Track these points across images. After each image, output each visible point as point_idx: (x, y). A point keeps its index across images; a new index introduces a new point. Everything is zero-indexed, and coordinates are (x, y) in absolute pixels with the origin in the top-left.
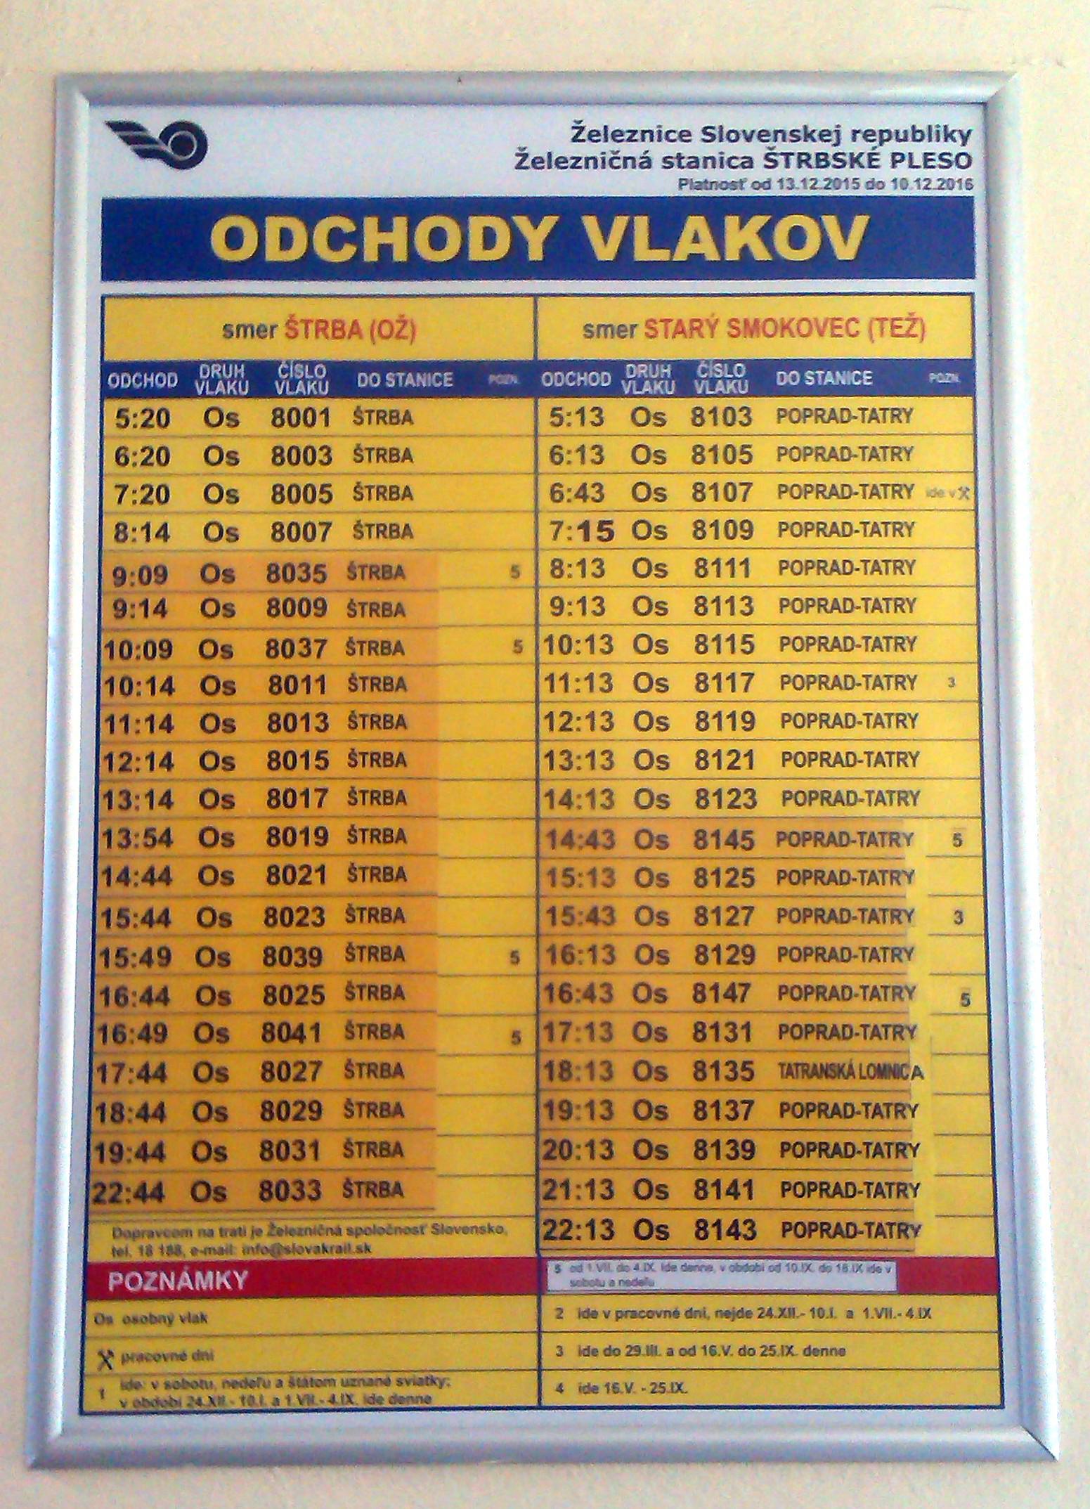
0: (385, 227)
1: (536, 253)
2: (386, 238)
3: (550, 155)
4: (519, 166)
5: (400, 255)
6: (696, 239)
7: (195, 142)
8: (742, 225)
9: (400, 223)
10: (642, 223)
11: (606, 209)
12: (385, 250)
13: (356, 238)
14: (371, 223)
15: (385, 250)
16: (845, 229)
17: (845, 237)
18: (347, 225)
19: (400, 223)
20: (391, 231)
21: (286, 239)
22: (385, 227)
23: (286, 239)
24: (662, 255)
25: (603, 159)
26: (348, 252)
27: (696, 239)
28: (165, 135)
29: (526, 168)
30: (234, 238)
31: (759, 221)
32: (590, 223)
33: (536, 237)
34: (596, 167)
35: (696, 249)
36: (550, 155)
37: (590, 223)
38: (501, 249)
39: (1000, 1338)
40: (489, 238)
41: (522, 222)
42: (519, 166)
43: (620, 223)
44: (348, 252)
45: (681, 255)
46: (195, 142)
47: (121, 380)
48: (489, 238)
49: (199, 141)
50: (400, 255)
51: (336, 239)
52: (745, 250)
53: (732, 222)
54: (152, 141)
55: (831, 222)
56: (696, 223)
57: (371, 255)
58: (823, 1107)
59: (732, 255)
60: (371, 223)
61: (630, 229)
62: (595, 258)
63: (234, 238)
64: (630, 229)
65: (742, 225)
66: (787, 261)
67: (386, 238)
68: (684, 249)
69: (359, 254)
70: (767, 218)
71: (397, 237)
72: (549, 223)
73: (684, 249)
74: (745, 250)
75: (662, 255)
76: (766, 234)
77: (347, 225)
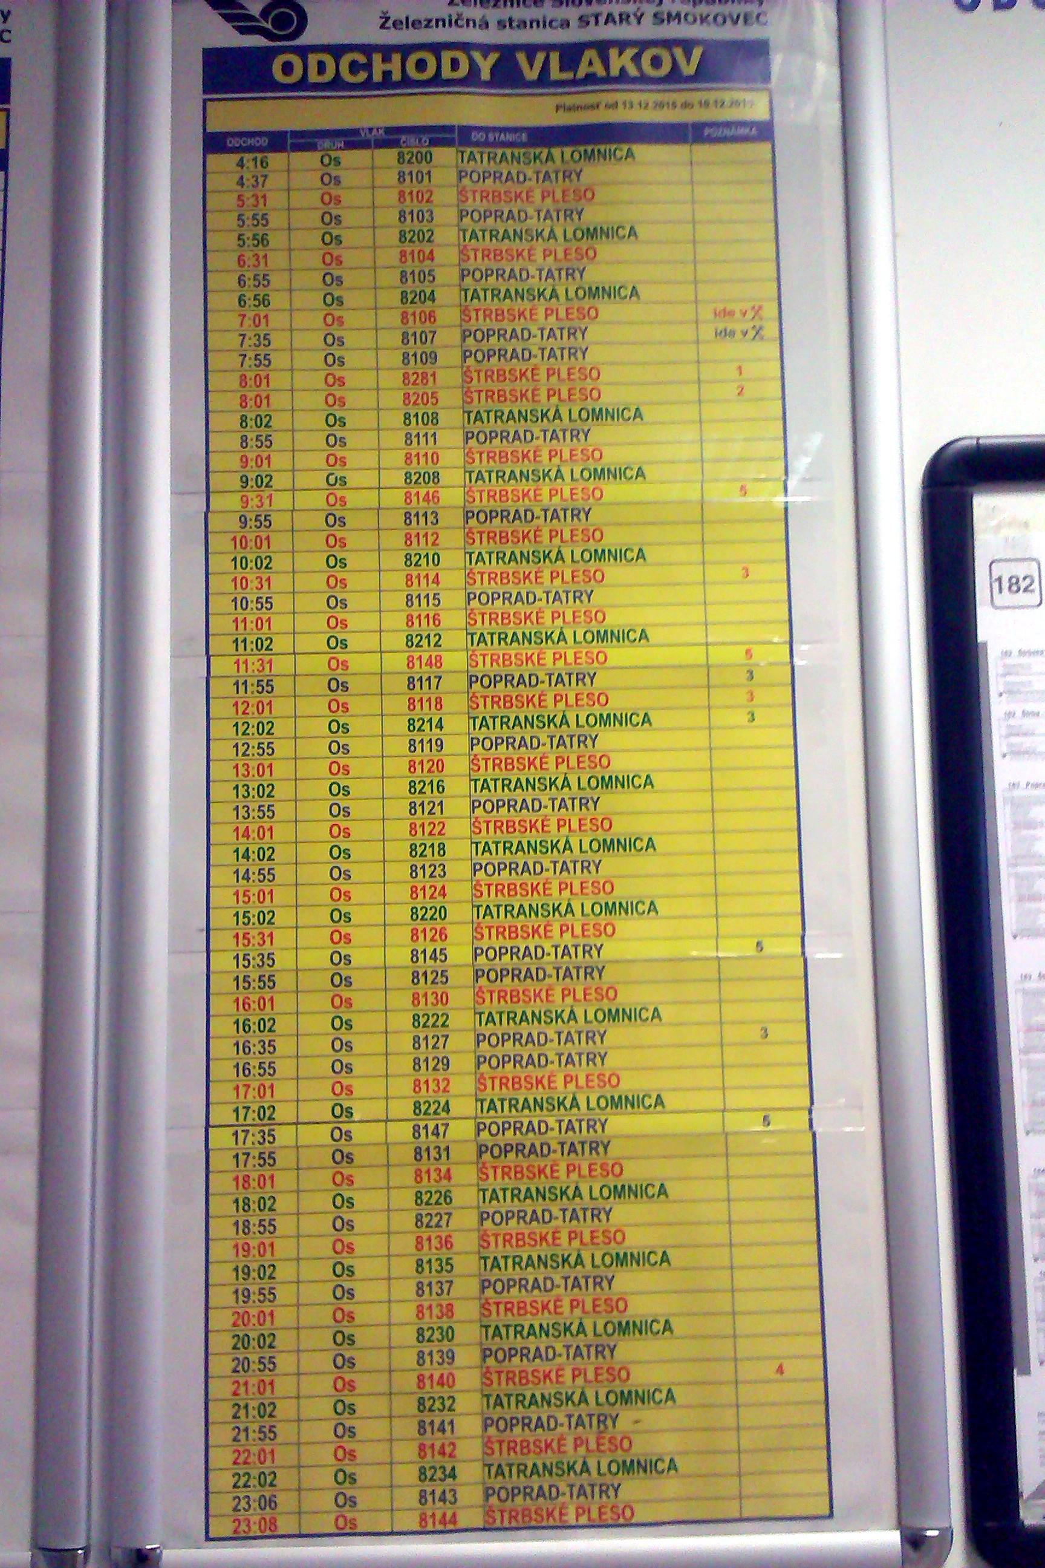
0: (386, 59)
1: (485, 75)
2: (387, 67)
3: (407, 19)
4: (382, 27)
5: (397, 76)
6: (591, 63)
7: (273, 14)
8: (620, 54)
9: (397, 58)
10: (555, 57)
11: (531, 50)
12: (387, 74)
13: (368, 67)
14: (377, 58)
15: (387, 74)
16: (688, 56)
17: (688, 61)
18: (362, 59)
19: (397, 58)
20: (9, 60)
21: (321, 68)
22: (386, 59)
23: (321, 68)
24: (568, 76)
25: (450, 21)
26: (362, 76)
27: (591, 63)
28: (265, 13)
29: (388, 28)
30: (287, 68)
31: (630, 52)
32: (521, 58)
33: (485, 67)
34: (444, 25)
35: (591, 70)
36: (407, 19)
37: (521, 58)
38: (463, 70)
39: (207, 465)
40: (455, 64)
41: (477, 56)
42: (382, 27)
43: (540, 57)
44: (362, 76)
45: (581, 73)
46: (273, 14)
47: (214, 143)
48: (455, 64)
49: (270, 13)
50: (397, 76)
51: (354, 67)
52: (623, 70)
53: (613, 53)
54: (251, 18)
55: (679, 52)
56: (590, 54)
57: (377, 77)
58: (505, 514)
59: (615, 72)
60: (377, 58)
61: (547, 62)
62: (524, 79)
63: (287, 68)
64: (547, 62)
65: (620, 54)
66: (271, 70)
67: (387, 67)
68: (583, 71)
69: (370, 77)
70: (636, 50)
71: (395, 66)
72: (493, 57)
73: (583, 71)
74: (623, 70)
75: (568, 76)
76: (636, 59)
77: (362, 59)
